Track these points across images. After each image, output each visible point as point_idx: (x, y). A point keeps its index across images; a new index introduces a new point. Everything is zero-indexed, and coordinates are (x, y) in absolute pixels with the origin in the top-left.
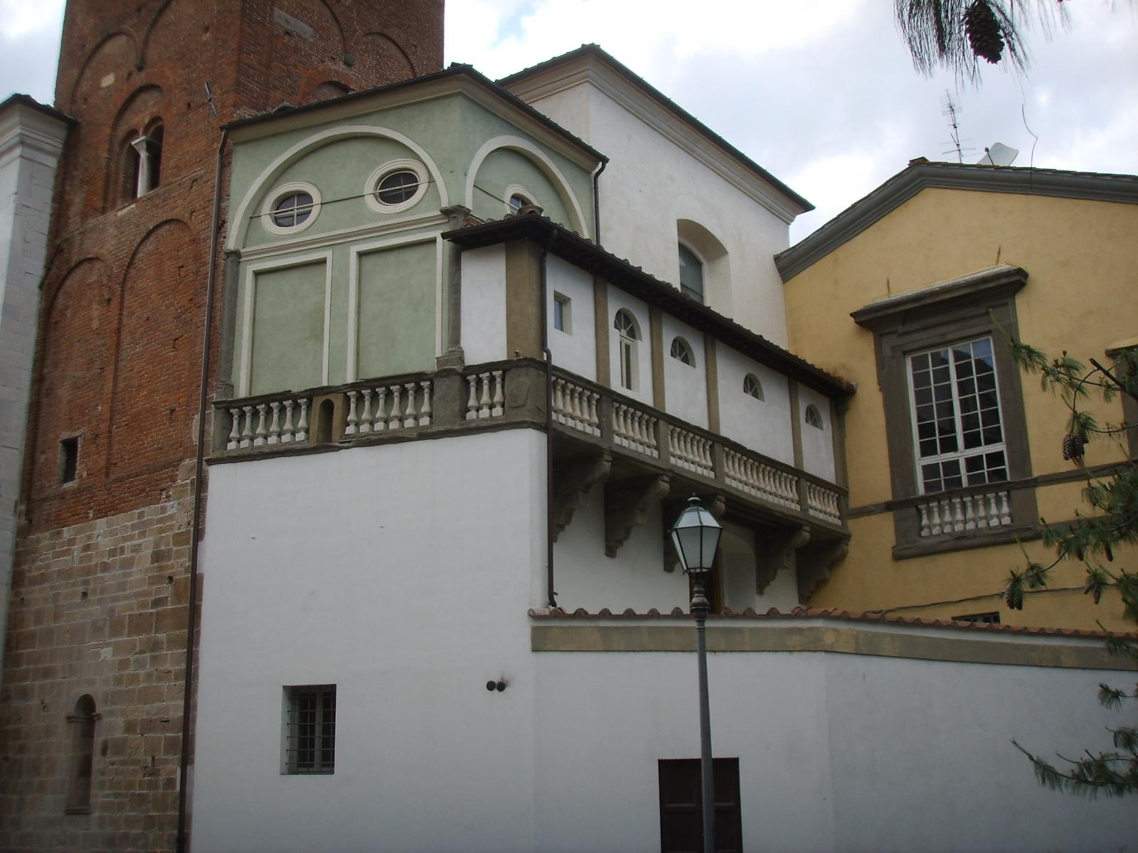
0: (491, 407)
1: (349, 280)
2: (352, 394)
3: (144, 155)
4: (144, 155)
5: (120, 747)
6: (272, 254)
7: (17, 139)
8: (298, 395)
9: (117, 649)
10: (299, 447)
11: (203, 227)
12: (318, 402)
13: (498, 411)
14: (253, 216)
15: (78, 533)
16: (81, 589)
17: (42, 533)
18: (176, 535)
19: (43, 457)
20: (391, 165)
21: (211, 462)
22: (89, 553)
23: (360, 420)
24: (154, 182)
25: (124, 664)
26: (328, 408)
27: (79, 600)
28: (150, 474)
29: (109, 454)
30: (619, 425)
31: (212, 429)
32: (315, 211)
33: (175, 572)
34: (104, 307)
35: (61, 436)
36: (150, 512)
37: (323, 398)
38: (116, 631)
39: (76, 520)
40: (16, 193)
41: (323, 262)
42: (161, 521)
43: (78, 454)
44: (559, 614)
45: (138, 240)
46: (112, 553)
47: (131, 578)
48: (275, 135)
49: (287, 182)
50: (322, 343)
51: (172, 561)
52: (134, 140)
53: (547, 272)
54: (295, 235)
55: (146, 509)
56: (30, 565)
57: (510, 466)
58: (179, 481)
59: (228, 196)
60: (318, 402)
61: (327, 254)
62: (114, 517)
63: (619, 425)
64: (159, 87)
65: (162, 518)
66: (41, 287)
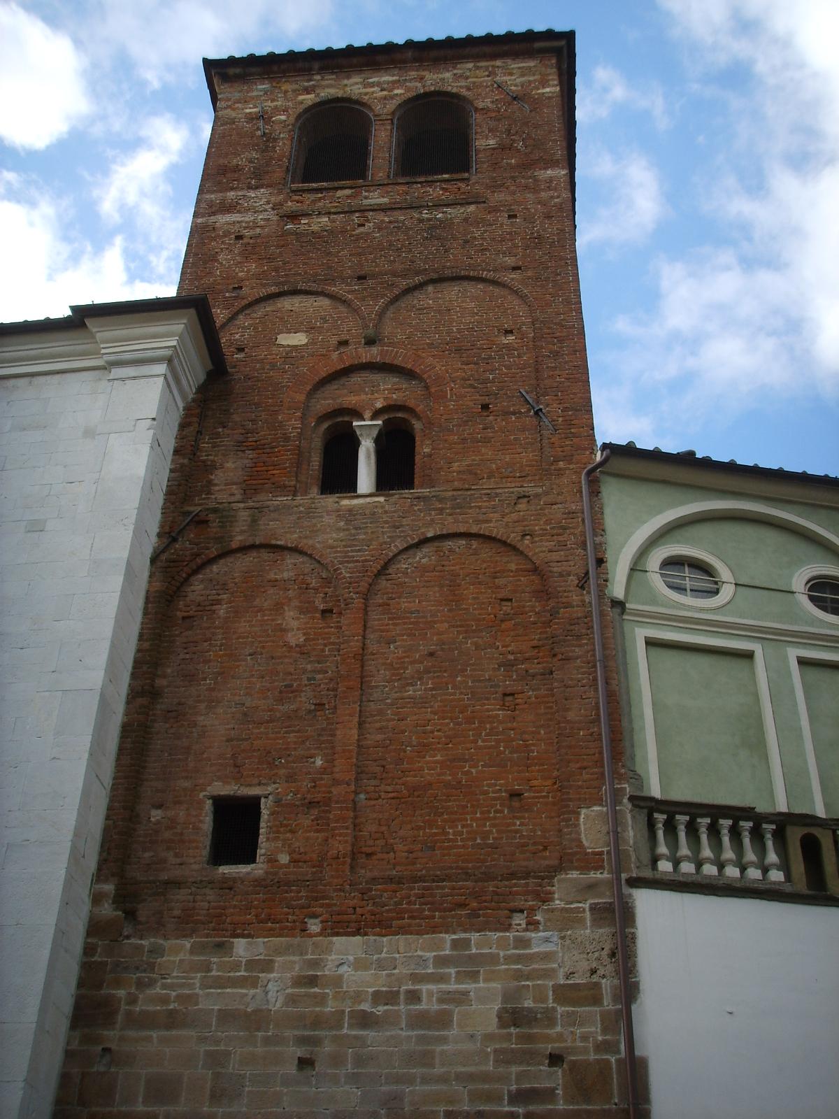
1: (793, 688)
6: (675, 624)
7: (168, 352)
8: (767, 818)
11: (558, 558)
12: (795, 835)
14: (636, 568)
15: (278, 951)
17: (165, 938)
18: (556, 988)
19: (156, 815)
20: (824, 569)
21: (636, 883)
22: (316, 990)
27: (292, 1069)
28: (476, 882)
29: (355, 837)
31: (631, 833)
33: (567, 1048)
34: (313, 618)
35: (209, 788)
36: (480, 942)
37: (806, 830)
39: (271, 929)
40: (154, 419)
41: (749, 656)
42: (518, 959)
43: (262, 824)
45: (401, 545)
47: (445, 1048)
48: (664, 482)
49: (678, 542)
50: (765, 757)
51: (559, 1029)
52: (357, 421)
53: (70, 818)
54: (702, 610)
55: (474, 936)
56: (133, 990)
58: (557, 902)
59: (603, 530)
60: (795, 835)
61: (757, 648)
62: (385, 939)
65: (519, 956)
66: (153, 561)
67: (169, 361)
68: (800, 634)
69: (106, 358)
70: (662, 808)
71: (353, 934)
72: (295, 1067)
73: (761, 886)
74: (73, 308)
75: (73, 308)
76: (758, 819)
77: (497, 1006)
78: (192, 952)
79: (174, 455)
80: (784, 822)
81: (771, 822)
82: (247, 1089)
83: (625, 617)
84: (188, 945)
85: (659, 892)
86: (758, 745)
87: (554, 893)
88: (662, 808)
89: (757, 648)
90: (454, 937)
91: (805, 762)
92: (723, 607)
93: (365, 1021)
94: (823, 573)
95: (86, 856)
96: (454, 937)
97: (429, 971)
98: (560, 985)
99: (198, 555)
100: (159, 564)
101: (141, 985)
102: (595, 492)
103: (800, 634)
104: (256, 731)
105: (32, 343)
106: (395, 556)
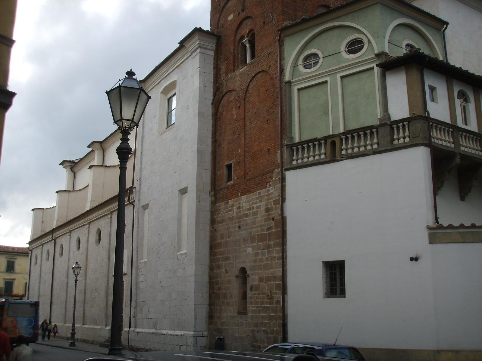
0: (404, 138)
2: (343, 137)
3: (248, 46)
4: (248, 46)
5: (257, 288)
7: (198, 45)
9: (254, 248)
10: (322, 161)
12: (329, 141)
13: (407, 140)
16: (238, 225)
17: (221, 203)
21: (287, 170)
23: (347, 148)
24: (253, 56)
25: (257, 254)
26: (333, 144)
27: (237, 229)
30: (463, 142)
32: (321, 61)
36: (263, 192)
37: (331, 140)
38: (253, 241)
40: (199, 67)
41: (326, 82)
42: (268, 195)
44: (441, 227)
46: (249, 209)
54: (313, 72)
55: (261, 191)
57: (414, 164)
60: (329, 141)
61: (328, 79)
63: (463, 142)
64: (251, 17)
66: (212, 104)
67: (200, 47)
68: (349, 65)
69: (190, 52)
70: (294, 145)
71: (244, 195)
72: (237, 228)
73: (302, 164)
74: (179, 43)
75: (179, 43)
76: (319, 140)
77: (264, 208)
78: (224, 205)
79: (214, 69)
80: (326, 138)
81: (322, 140)
82: (232, 234)
83: (292, 84)
84: (223, 203)
85: (293, 171)
86: (326, 113)
87: (273, 176)
88: (294, 145)
89: (328, 79)
90: (259, 192)
91: (339, 114)
92: (319, 68)
93: (247, 215)
94: (349, 40)
95: (204, 188)
96: (259, 192)
97: (255, 201)
98: (274, 200)
99: (219, 98)
100: (214, 104)
101: (219, 214)
102: (281, 45)
103: (349, 65)
104: (231, 146)
105: (175, 57)
106: (249, 84)
